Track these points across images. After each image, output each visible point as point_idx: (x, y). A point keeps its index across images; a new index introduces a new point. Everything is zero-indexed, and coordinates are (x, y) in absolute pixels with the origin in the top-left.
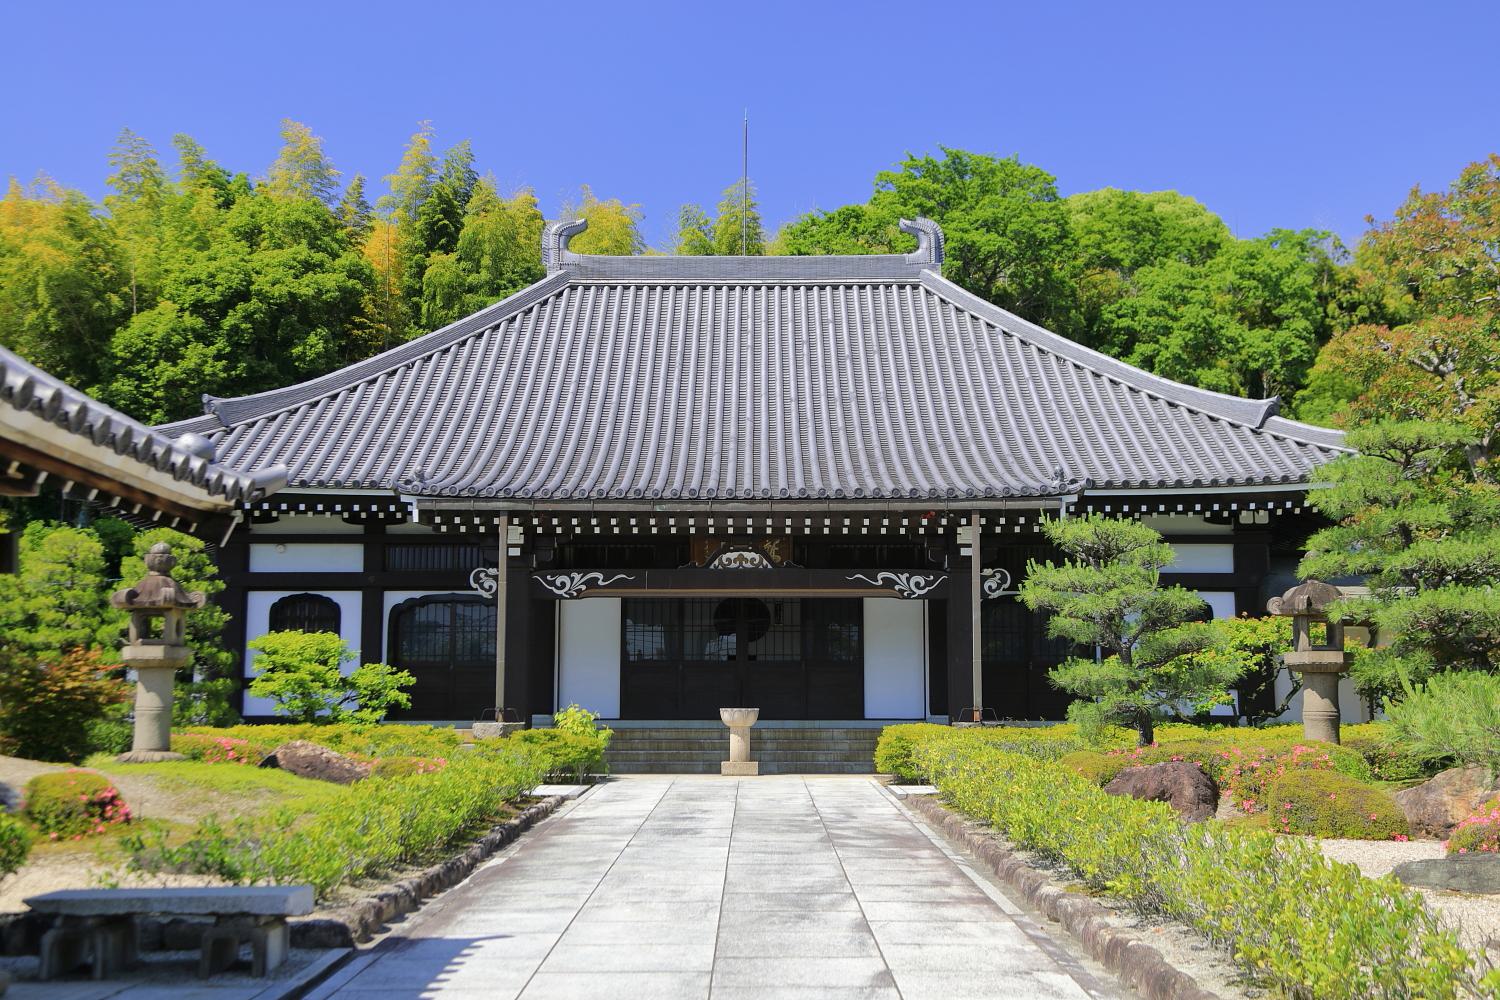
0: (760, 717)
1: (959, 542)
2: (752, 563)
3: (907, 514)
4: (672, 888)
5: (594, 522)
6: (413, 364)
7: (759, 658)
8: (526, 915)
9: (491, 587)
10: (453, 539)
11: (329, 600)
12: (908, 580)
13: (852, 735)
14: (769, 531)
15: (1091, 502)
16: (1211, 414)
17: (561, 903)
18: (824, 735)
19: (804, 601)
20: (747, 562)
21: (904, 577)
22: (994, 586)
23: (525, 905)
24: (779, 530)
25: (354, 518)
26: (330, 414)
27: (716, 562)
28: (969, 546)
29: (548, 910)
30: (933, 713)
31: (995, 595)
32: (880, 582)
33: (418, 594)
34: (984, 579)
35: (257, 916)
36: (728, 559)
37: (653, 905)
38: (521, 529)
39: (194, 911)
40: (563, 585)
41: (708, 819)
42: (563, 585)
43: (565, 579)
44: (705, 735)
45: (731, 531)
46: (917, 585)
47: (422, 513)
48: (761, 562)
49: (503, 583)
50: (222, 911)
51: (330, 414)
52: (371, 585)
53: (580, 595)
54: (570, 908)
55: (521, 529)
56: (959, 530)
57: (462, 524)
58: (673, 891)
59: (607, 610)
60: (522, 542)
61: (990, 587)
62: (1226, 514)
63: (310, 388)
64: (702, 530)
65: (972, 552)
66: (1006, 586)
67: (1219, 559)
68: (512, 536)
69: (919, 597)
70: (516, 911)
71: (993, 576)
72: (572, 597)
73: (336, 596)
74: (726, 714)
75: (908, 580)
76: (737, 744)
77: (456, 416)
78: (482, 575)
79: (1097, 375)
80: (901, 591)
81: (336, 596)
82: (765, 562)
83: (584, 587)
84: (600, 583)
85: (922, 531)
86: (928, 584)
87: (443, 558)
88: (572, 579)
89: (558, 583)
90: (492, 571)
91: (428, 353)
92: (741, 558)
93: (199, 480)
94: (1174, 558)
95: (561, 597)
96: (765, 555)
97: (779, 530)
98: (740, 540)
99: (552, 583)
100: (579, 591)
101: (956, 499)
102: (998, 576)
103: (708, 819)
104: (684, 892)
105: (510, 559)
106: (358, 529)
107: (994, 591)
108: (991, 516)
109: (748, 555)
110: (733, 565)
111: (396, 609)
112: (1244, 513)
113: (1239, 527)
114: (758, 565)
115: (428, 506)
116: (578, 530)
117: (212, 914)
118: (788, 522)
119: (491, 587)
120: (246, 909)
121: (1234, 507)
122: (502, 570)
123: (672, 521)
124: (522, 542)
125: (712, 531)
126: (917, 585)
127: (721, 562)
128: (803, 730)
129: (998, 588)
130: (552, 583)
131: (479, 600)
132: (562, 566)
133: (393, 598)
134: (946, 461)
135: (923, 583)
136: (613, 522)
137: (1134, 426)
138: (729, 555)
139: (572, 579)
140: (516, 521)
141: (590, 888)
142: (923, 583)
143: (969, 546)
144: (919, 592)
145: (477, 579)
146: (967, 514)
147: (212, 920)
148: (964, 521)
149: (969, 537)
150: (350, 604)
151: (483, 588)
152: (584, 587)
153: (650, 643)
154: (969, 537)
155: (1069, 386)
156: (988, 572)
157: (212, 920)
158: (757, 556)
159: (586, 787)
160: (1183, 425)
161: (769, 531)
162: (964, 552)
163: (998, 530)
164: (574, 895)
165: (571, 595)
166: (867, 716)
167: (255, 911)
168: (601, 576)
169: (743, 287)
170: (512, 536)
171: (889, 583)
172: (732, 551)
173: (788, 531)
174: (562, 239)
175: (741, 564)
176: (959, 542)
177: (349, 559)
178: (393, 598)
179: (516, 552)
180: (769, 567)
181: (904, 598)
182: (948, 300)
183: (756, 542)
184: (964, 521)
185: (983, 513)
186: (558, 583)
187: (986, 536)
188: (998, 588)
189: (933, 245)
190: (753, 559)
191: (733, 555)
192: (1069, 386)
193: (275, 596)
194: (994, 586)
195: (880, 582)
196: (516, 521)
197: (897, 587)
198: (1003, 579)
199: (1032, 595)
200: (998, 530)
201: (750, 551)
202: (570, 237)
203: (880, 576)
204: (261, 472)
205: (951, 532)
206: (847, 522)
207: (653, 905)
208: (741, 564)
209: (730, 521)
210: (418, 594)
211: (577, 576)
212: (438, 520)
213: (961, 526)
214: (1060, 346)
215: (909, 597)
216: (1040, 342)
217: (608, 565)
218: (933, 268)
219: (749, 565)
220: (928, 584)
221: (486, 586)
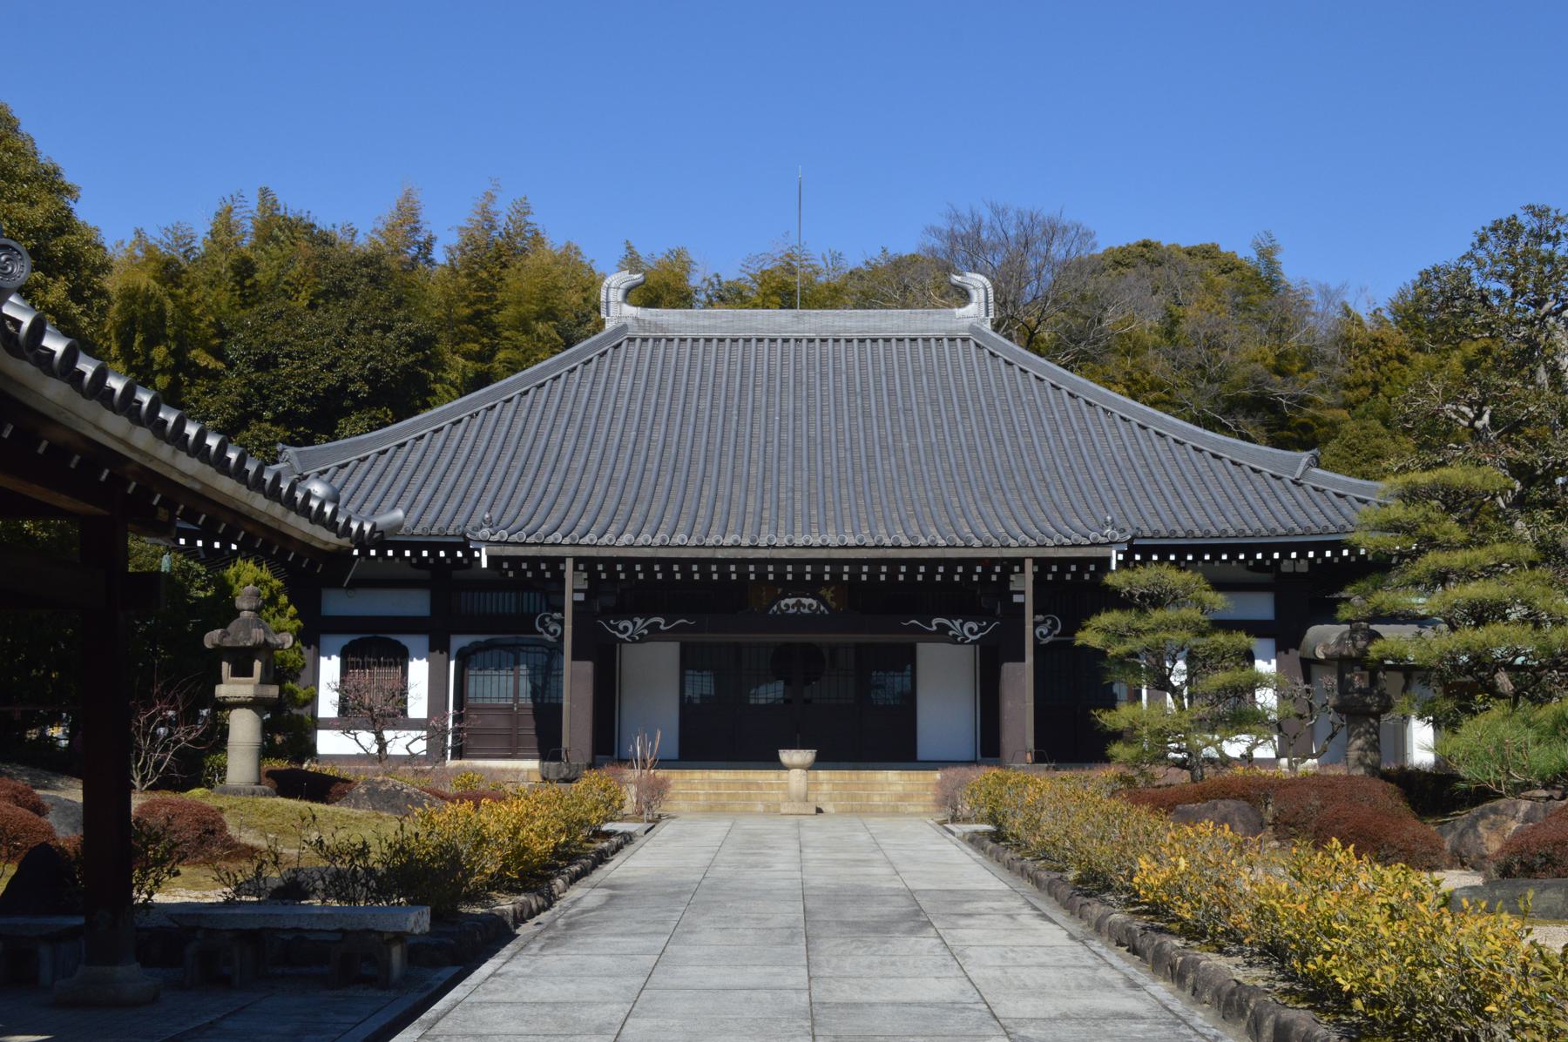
1: (1012, 588)
3: (961, 561)
4: (755, 915)
5: (657, 568)
8: (620, 939)
9: (556, 631)
10: (520, 585)
11: (397, 643)
12: (962, 626)
14: (827, 577)
15: (1140, 551)
16: (1253, 466)
17: (652, 928)
19: (858, 646)
21: (957, 623)
22: (1045, 632)
23: (618, 930)
24: (836, 576)
26: (398, 463)
27: (775, 608)
28: (1023, 592)
29: (642, 934)
30: (983, 755)
31: (1046, 641)
32: (935, 628)
33: (482, 638)
34: (1036, 625)
35: (381, 933)
36: (787, 605)
37: (740, 931)
39: (323, 927)
40: (626, 629)
41: (776, 855)
42: (626, 629)
43: (628, 624)
45: (789, 577)
46: (971, 630)
47: (490, 558)
48: (818, 607)
49: (568, 627)
50: (349, 928)
51: (398, 463)
53: (642, 639)
54: (665, 933)
56: (1012, 577)
57: (528, 569)
58: (757, 919)
59: (668, 653)
60: (586, 587)
61: (1041, 633)
62: (1268, 563)
63: (378, 437)
65: (1028, 600)
66: (1057, 632)
67: (1261, 607)
68: (573, 586)
69: (973, 642)
70: (611, 935)
71: (1044, 622)
72: (634, 641)
75: (962, 626)
78: (547, 620)
80: (955, 637)
82: (822, 608)
83: (646, 632)
84: (662, 627)
85: (975, 578)
86: (981, 629)
87: (504, 603)
88: (635, 624)
89: (621, 627)
90: (557, 615)
91: (491, 404)
92: (799, 604)
93: (331, 525)
94: (1220, 602)
95: (624, 641)
96: (821, 600)
97: (836, 576)
98: (799, 587)
99: (615, 628)
100: (641, 635)
102: (1049, 622)
103: (776, 855)
104: (767, 919)
105: (575, 603)
107: (1045, 637)
112: (1285, 562)
113: (1282, 576)
115: (497, 550)
116: (641, 576)
117: (340, 930)
118: (846, 569)
119: (556, 631)
120: (371, 927)
121: (1276, 555)
123: (714, 568)
124: (586, 587)
125: (771, 577)
126: (971, 630)
129: (1049, 634)
130: (615, 628)
131: (544, 643)
132: (626, 610)
135: (976, 629)
136: (619, 567)
139: (635, 624)
140: (581, 567)
141: (677, 916)
142: (976, 629)
143: (1023, 592)
144: (972, 638)
145: (542, 623)
146: (1020, 561)
147: (339, 936)
148: (1017, 569)
149: (1024, 586)
151: (548, 632)
152: (646, 632)
153: (702, 685)
154: (1024, 586)
156: (1040, 618)
157: (339, 936)
158: (814, 602)
161: (827, 577)
162: (1017, 599)
163: (994, 578)
164: (664, 922)
165: (634, 639)
167: (379, 928)
168: (662, 621)
170: (573, 586)
171: (943, 629)
173: (845, 577)
176: (1012, 588)
177: (416, 603)
179: (580, 597)
181: (958, 643)
182: (997, 353)
183: (813, 588)
184: (1017, 569)
185: (1036, 561)
186: (621, 627)
187: (1039, 580)
188: (1049, 634)
190: (811, 605)
191: (791, 601)
193: (345, 640)
194: (1045, 632)
195: (935, 628)
196: (581, 567)
197: (951, 633)
198: (1054, 626)
199: (1089, 637)
200: (1050, 577)
203: (935, 621)
204: (384, 519)
206: (884, 569)
207: (740, 931)
209: (770, 568)
210: (482, 638)
211: (639, 621)
212: (505, 565)
213: (1014, 573)
214: (1107, 399)
215: (962, 642)
216: (1088, 395)
217: (670, 614)
220: (981, 629)
221: (551, 629)
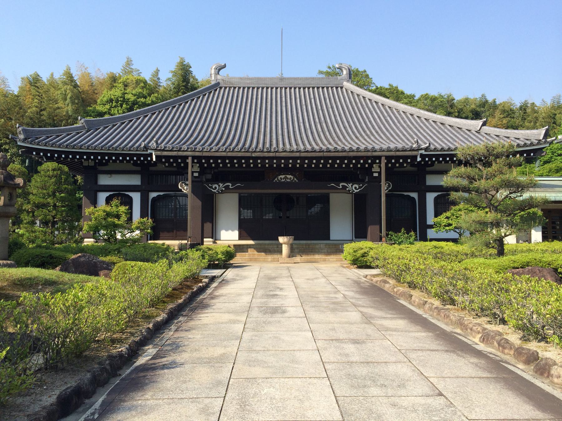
0: (295, 239)
1: (373, 170)
2: (290, 180)
6: (162, 111)
7: (290, 217)
12: (352, 186)
13: (328, 247)
18: (317, 246)
20: (288, 179)
21: (350, 185)
25: (135, 164)
27: (276, 179)
32: (341, 187)
36: (281, 178)
38: (198, 165)
40: (216, 188)
42: (216, 188)
43: (217, 186)
44: (271, 247)
46: (355, 188)
47: (156, 157)
48: (294, 179)
52: (144, 190)
55: (198, 165)
56: (374, 165)
64: (271, 166)
73: (131, 194)
74: (281, 239)
75: (352, 186)
76: (285, 249)
77: (176, 127)
79: (412, 115)
80: (349, 190)
81: (131, 194)
83: (224, 189)
84: (230, 187)
86: (360, 187)
88: (219, 186)
89: (214, 187)
92: (286, 178)
98: (286, 170)
99: (211, 187)
100: (222, 190)
101: (375, 151)
106: (139, 168)
108: (389, 158)
109: (289, 176)
110: (283, 180)
111: (154, 199)
114: (292, 180)
115: (159, 153)
122: (189, 182)
126: (355, 188)
127: (278, 179)
128: (309, 245)
130: (211, 187)
132: (216, 179)
133: (153, 195)
134: (393, 125)
135: (358, 187)
137: (431, 131)
138: (281, 176)
139: (219, 186)
142: (358, 187)
150: (136, 197)
152: (224, 189)
155: (403, 118)
158: (292, 177)
159: (225, 270)
160: (449, 130)
165: (219, 192)
166: (331, 239)
168: (231, 185)
169: (281, 88)
171: (344, 187)
172: (282, 175)
174: (217, 70)
175: (286, 180)
176: (373, 170)
178: (153, 195)
179: (196, 174)
180: (297, 181)
186: (214, 187)
189: (348, 73)
190: (291, 178)
191: (283, 176)
192: (403, 118)
195: (341, 187)
197: (347, 189)
201: (289, 175)
202: (219, 70)
203: (341, 184)
205: (371, 166)
208: (286, 180)
210: (161, 194)
211: (221, 185)
218: (348, 81)
219: (289, 180)
220: (360, 187)
